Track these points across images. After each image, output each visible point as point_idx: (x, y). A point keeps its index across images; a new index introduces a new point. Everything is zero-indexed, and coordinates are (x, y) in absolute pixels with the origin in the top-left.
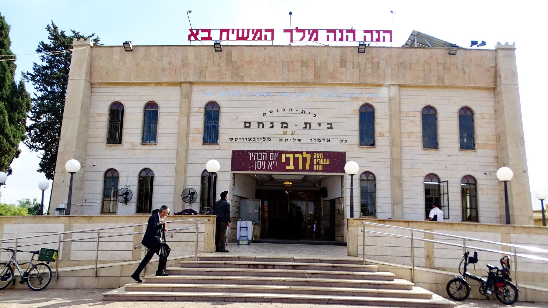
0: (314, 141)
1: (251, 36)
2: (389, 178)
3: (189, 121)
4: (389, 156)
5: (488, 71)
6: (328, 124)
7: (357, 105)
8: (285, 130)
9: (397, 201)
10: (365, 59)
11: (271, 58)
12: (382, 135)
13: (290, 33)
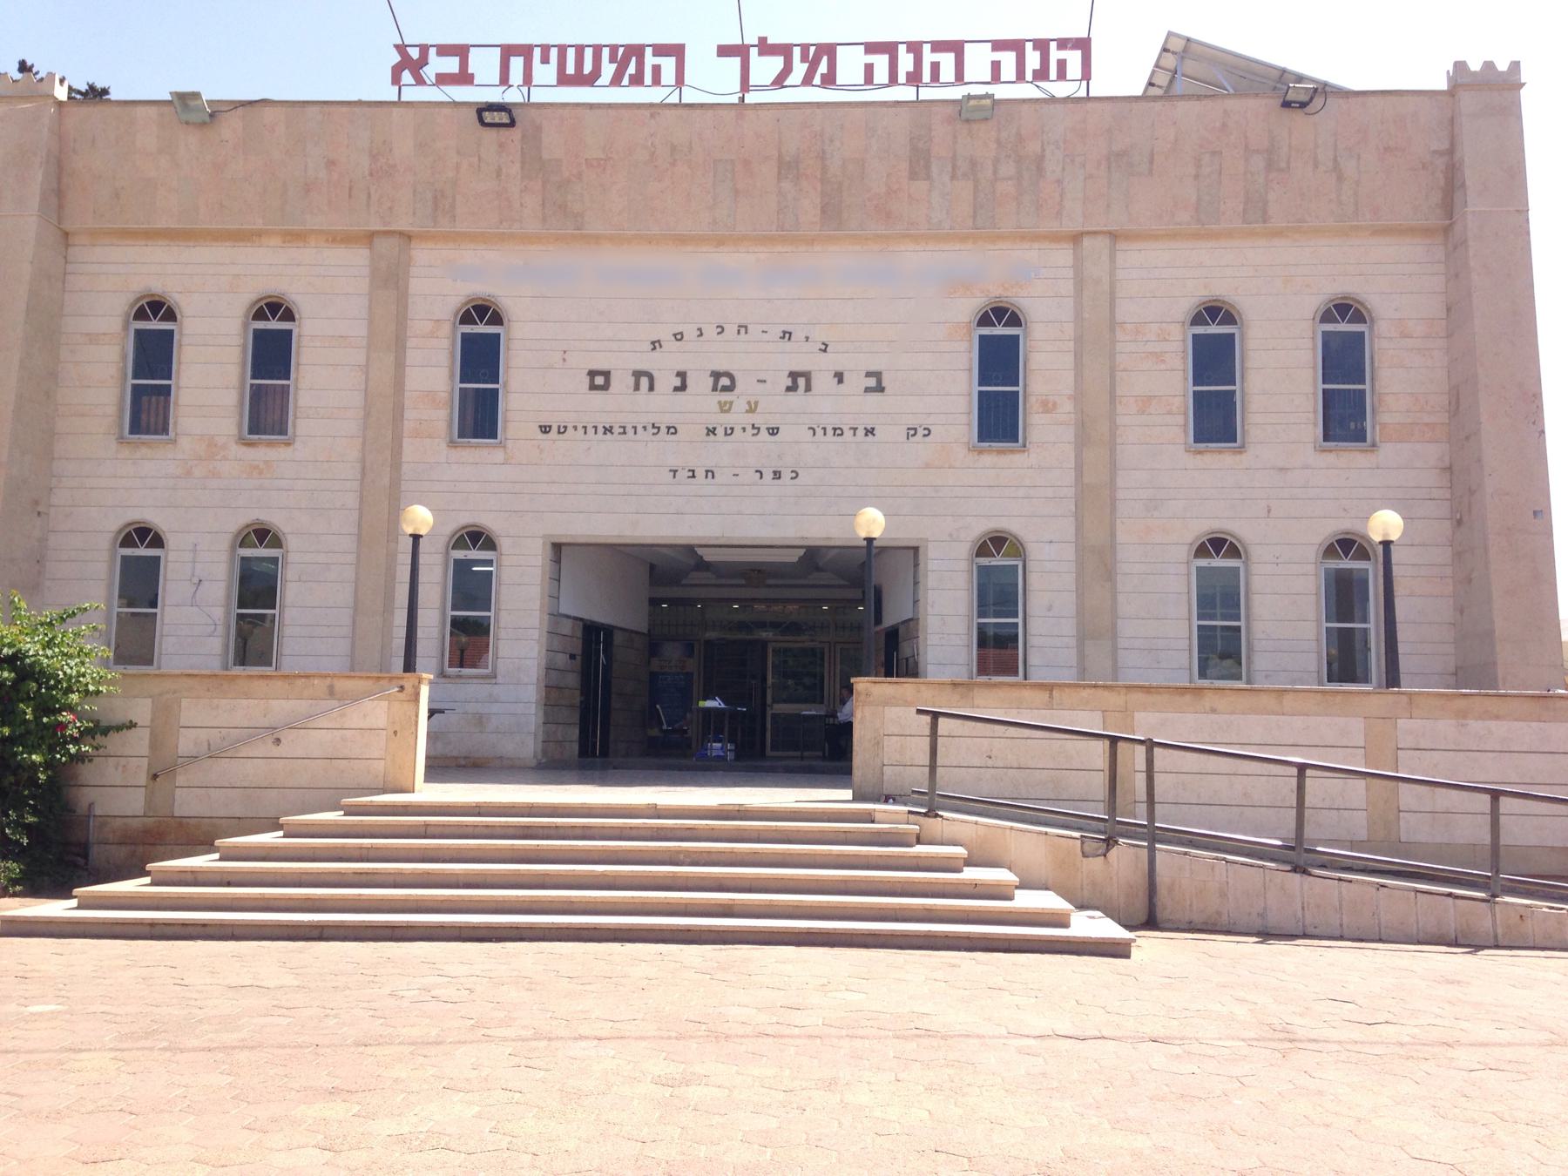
0: (819, 432)
1: (608, 70)
2: (1069, 553)
3: (400, 365)
4: (1070, 477)
5: (1424, 167)
6: (869, 374)
7: (968, 307)
8: (726, 397)
9: (1096, 629)
10: (993, 146)
11: (673, 149)
12: (1048, 407)
13: (736, 62)
